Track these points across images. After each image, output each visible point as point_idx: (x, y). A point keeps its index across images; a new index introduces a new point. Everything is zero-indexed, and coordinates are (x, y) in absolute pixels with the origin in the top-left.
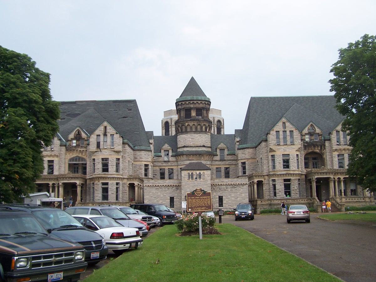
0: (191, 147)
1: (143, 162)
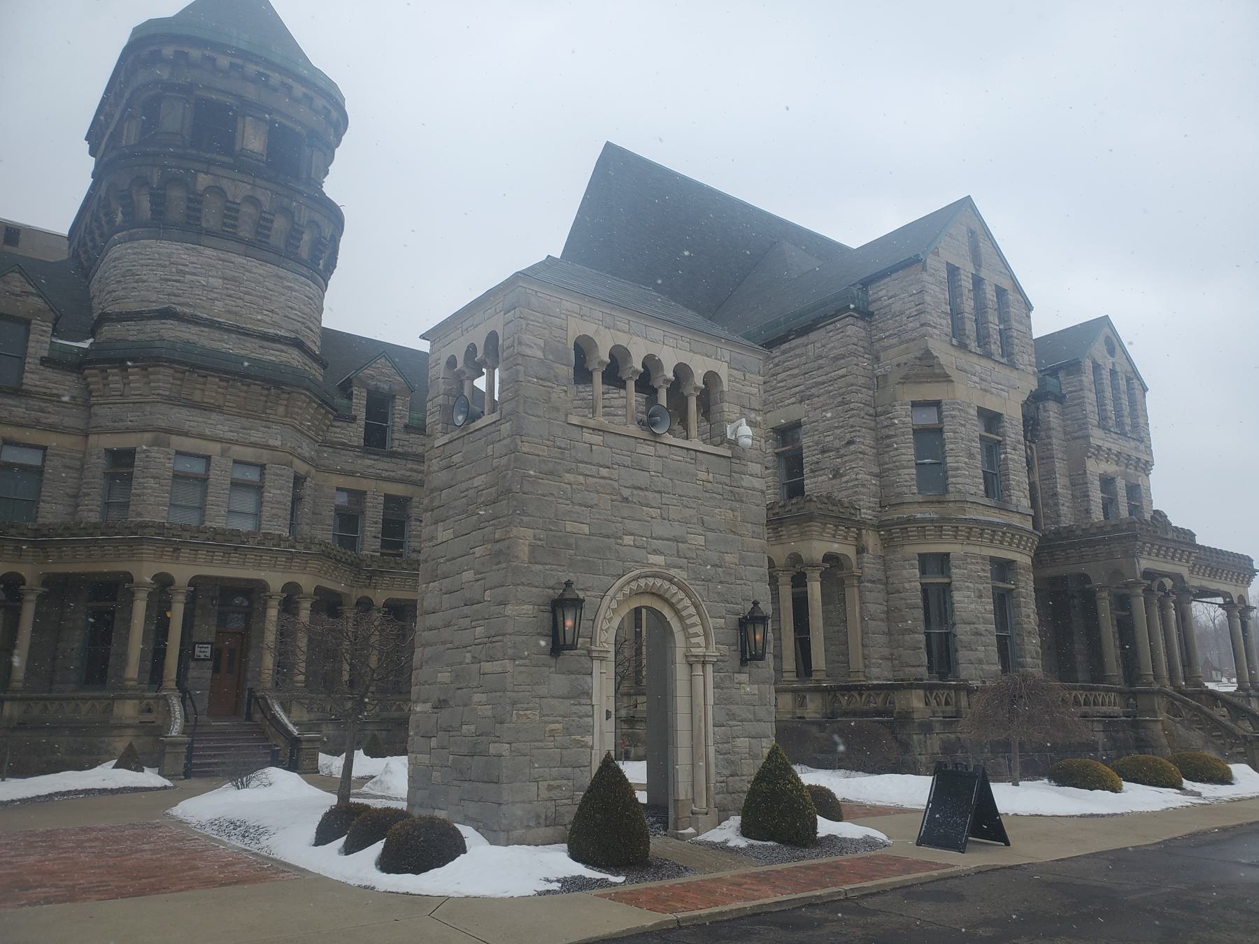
0: (212, 324)
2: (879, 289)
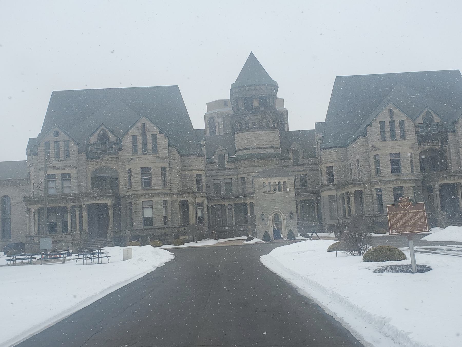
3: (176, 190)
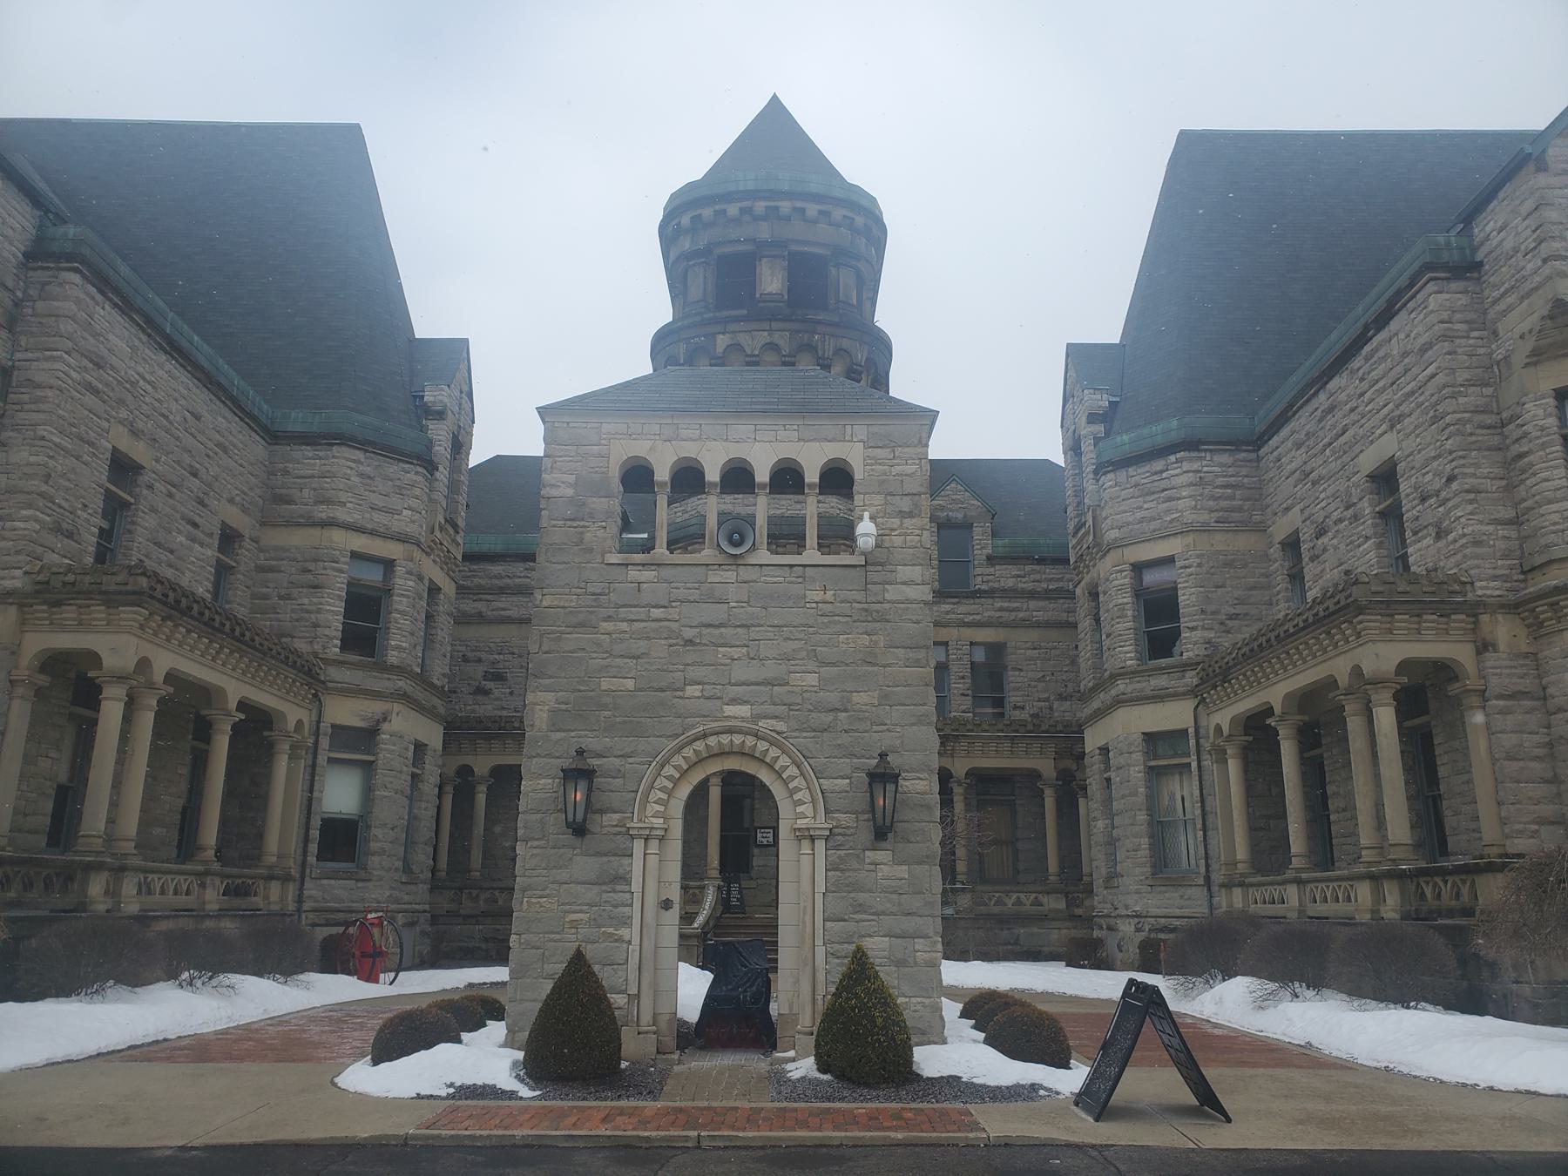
1: (338, 536)
2: (1485, 222)
3: (18, 573)
